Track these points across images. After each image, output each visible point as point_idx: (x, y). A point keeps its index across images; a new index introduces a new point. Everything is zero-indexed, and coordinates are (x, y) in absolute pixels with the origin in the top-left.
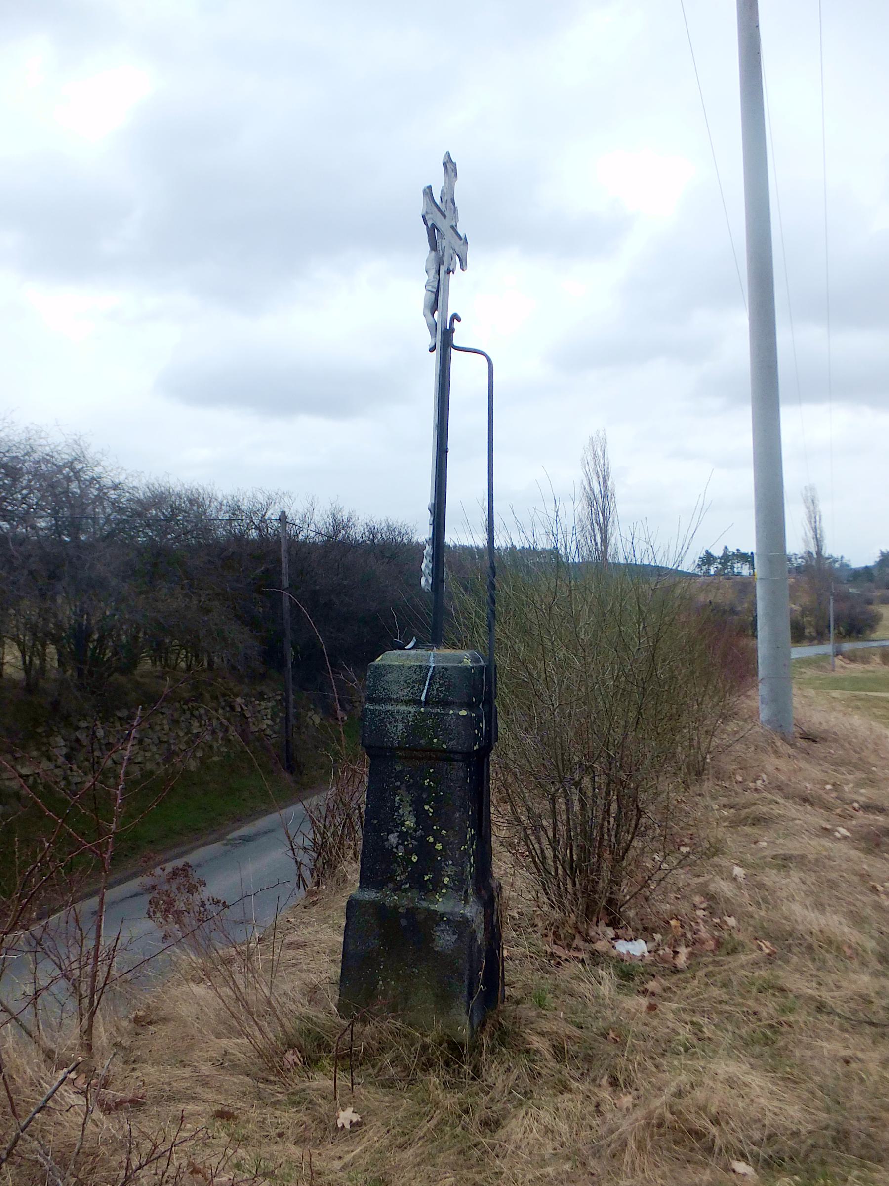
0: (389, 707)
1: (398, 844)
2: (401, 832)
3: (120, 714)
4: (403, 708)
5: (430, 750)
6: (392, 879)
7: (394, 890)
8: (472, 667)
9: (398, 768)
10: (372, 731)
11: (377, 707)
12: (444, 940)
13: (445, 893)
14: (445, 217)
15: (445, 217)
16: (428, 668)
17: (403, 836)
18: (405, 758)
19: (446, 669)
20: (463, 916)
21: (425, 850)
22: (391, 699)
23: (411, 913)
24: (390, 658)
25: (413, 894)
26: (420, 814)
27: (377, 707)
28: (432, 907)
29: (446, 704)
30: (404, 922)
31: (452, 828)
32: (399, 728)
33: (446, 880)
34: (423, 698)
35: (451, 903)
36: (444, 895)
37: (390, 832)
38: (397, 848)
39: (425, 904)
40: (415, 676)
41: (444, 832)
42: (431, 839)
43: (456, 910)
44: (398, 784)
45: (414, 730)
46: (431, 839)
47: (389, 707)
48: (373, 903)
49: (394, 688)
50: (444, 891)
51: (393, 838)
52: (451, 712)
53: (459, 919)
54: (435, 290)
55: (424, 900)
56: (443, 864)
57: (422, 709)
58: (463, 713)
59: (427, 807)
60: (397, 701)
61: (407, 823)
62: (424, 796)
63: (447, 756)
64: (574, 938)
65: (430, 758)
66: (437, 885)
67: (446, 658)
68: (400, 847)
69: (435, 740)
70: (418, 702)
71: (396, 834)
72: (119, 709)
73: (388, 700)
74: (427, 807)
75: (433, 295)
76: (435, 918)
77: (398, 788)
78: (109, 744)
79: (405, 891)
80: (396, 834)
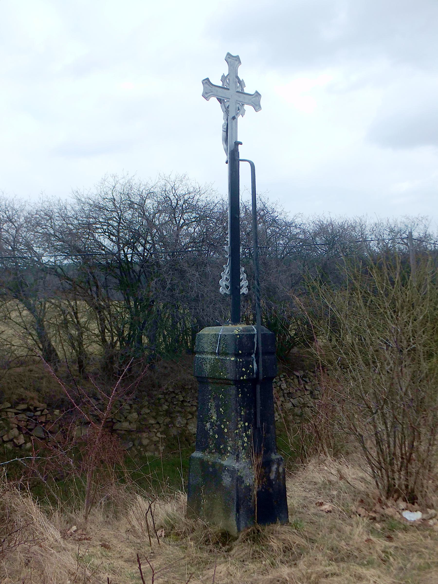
0: (204, 356)
1: (210, 429)
2: (211, 422)
3: (297, 374)
4: (209, 356)
5: (220, 379)
6: (208, 447)
7: (209, 453)
8: (238, 335)
9: (210, 388)
10: (197, 369)
11: (200, 356)
12: (227, 480)
13: (229, 456)
14: (228, 89)
15: (228, 89)
16: (218, 335)
17: (212, 424)
18: (212, 383)
19: (226, 336)
20: (234, 468)
21: (220, 432)
22: (205, 352)
23: (214, 464)
24: (207, 331)
25: (217, 455)
26: (218, 412)
27: (200, 356)
28: (222, 462)
29: (226, 354)
30: (211, 469)
31: (231, 421)
32: (208, 367)
33: (229, 448)
34: (217, 351)
35: (230, 461)
36: (228, 456)
37: (207, 422)
38: (210, 431)
39: (220, 461)
40: (214, 340)
41: (228, 423)
42: (223, 427)
43: (232, 464)
44: (210, 396)
45: (214, 368)
46: (223, 427)
47: (204, 356)
48: (199, 459)
49: (206, 346)
50: (228, 454)
51: (208, 425)
52: (228, 358)
53: (232, 469)
54: (225, 130)
55: (220, 459)
56: (228, 440)
57: (217, 357)
58: (233, 359)
59: (221, 409)
60: (207, 353)
61: (214, 417)
62: (220, 403)
63: (226, 382)
64: (375, 505)
65: (221, 383)
66: (226, 451)
67: (227, 330)
68: (211, 430)
69: (222, 374)
70: (215, 353)
71: (209, 423)
72: (297, 371)
73: (203, 352)
74: (221, 409)
75: (225, 133)
76: (223, 468)
77: (210, 399)
78: (290, 393)
79: (213, 453)
80: (209, 423)
